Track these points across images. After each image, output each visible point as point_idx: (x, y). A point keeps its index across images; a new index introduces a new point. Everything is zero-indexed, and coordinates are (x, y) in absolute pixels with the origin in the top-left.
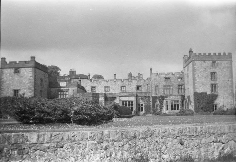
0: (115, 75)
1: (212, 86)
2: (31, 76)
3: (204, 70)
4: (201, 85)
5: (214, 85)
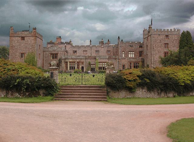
0: (91, 41)
1: (165, 54)
2: (33, 43)
3: (160, 41)
4: (157, 52)
5: (166, 53)
